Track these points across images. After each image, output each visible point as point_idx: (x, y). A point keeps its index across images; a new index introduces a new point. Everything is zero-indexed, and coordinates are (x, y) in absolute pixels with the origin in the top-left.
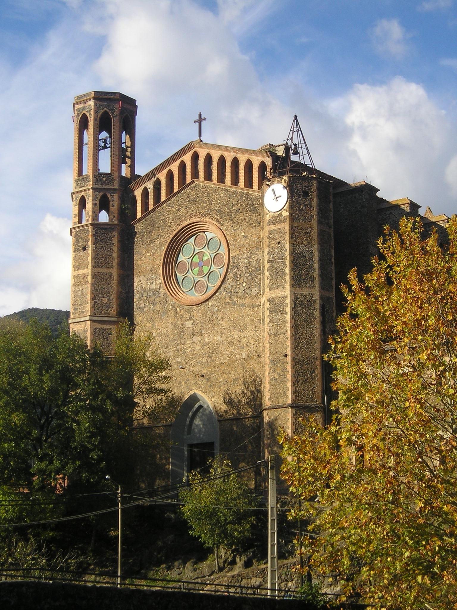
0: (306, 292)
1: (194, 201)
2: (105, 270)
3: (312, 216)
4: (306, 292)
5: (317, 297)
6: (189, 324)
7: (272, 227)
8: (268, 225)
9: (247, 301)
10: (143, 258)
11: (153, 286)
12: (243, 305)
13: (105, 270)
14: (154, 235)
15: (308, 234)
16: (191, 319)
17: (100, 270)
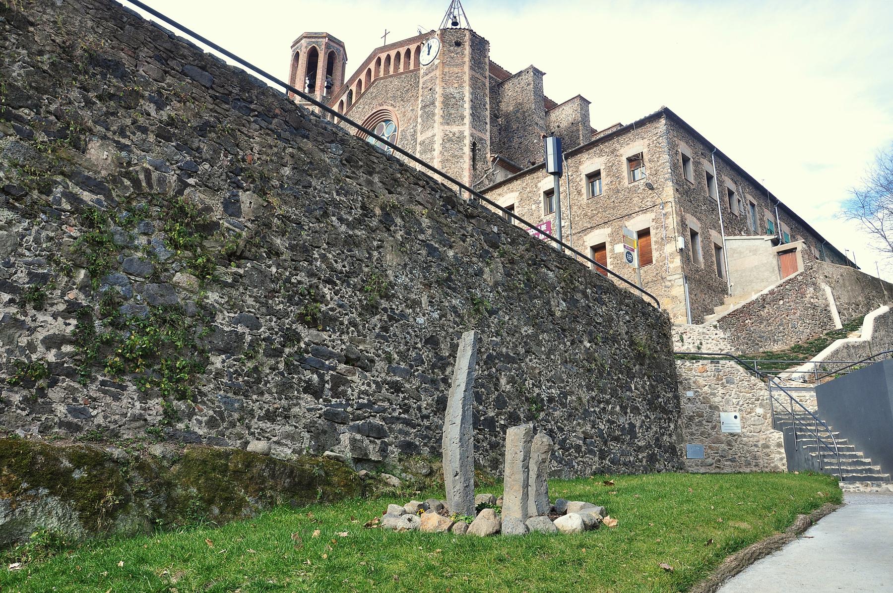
0: (455, 129)
3: (464, 63)
5: (467, 133)
7: (426, 78)
15: (459, 78)
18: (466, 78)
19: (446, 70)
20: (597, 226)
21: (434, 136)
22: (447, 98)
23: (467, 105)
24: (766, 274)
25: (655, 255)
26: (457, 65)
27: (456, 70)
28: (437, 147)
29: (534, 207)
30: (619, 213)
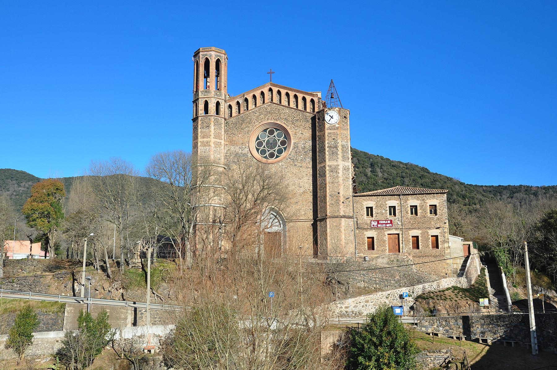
2: (218, 141)
4: (346, 164)
7: (329, 131)
8: (327, 129)
10: (237, 137)
11: (243, 152)
13: (218, 141)
14: (244, 126)
17: (216, 140)
20: (415, 229)
24: (459, 251)
25: (440, 246)
28: (340, 171)
29: (383, 211)
30: (425, 226)
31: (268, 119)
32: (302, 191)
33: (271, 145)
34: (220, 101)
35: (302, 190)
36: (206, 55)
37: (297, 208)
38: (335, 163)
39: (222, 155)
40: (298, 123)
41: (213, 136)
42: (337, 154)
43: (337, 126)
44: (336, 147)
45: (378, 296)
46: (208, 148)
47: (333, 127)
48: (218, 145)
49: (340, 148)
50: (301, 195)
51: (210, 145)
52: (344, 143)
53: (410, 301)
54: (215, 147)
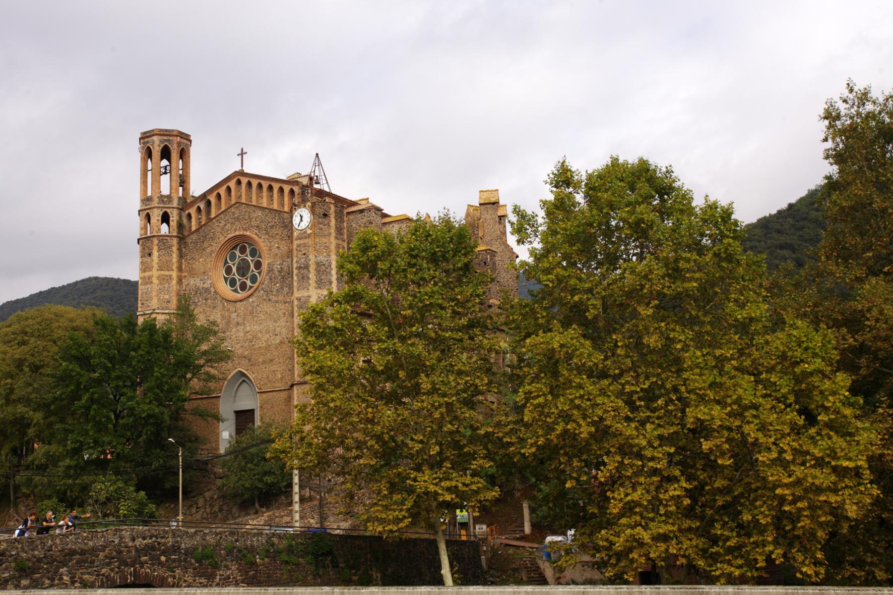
1: (238, 219)
2: (167, 273)
3: (330, 234)
6: (234, 315)
7: (299, 242)
8: (296, 239)
9: (281, 298)
11: (206, 286)
12: (277, 302)
13: (167, 273)
14: (206, 245)
15: (327, 248)
16: (235, 311)
17: (162, 272)
18: (333, 247)
19: (317, 240)
21: (310, 297)
22: (318, 264)
23: (334, 272)
26: (324, 236)
27: (325, 240)
31: (235, 230)
32: (278, 341)
33: (243, 269)
34: (168, 211)
35: (278, 340)
36: (148, 142)
37: (272, 368)
38: (306, 294)
39: (174, 294)
40: (274, 231)
41: (156, 266)
42: (308, 278)
43: (309, 231)
44: (307, 267)
45: (126, 534)
46: (149, 286)
47: (303, 235)
48: (163, 280)
49: (312, 268)
50: (277, 348)
51: (152, 282)
52: (321, 258)
53: (617, 492)
54: (161, 284)
